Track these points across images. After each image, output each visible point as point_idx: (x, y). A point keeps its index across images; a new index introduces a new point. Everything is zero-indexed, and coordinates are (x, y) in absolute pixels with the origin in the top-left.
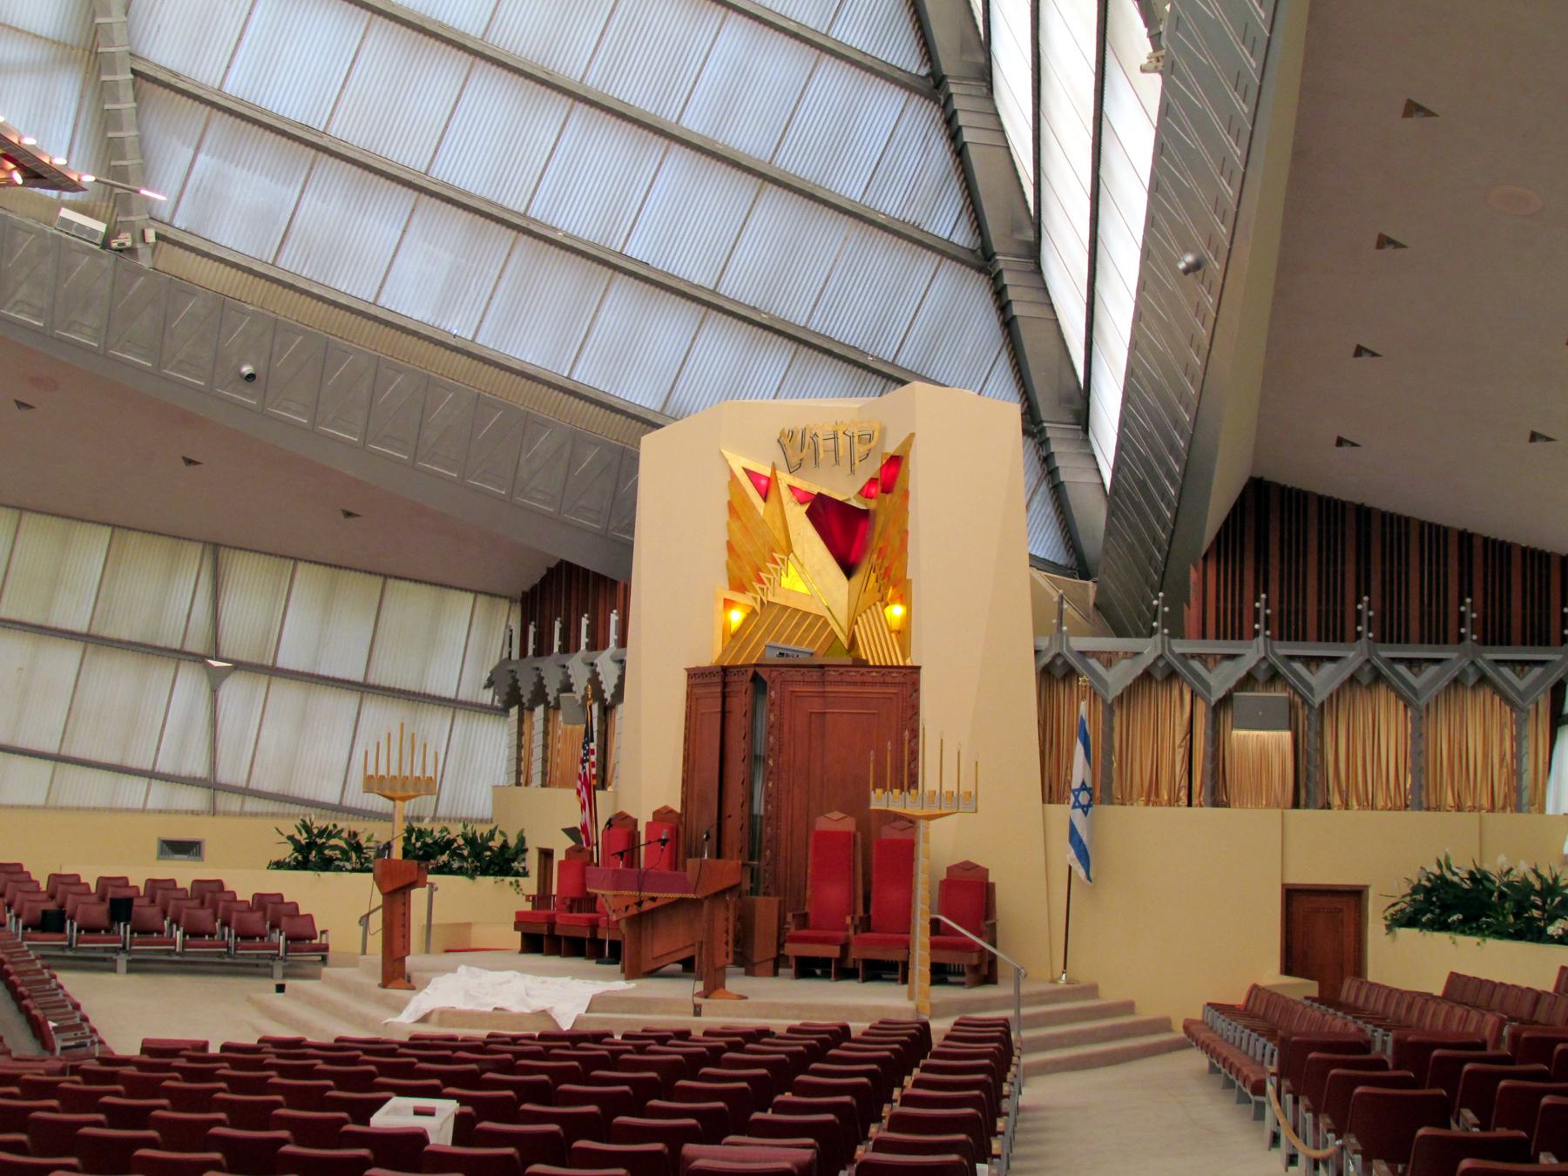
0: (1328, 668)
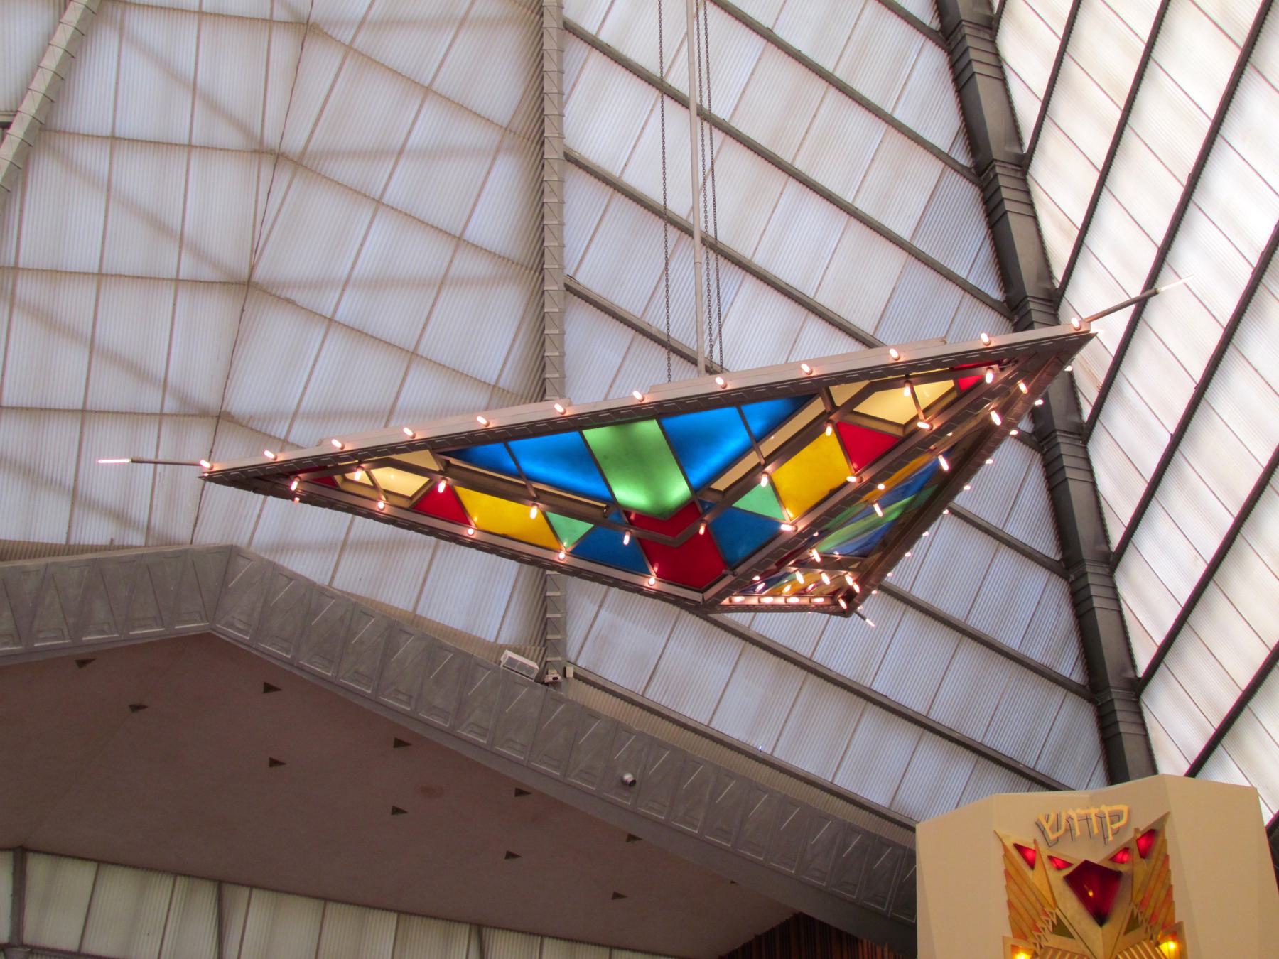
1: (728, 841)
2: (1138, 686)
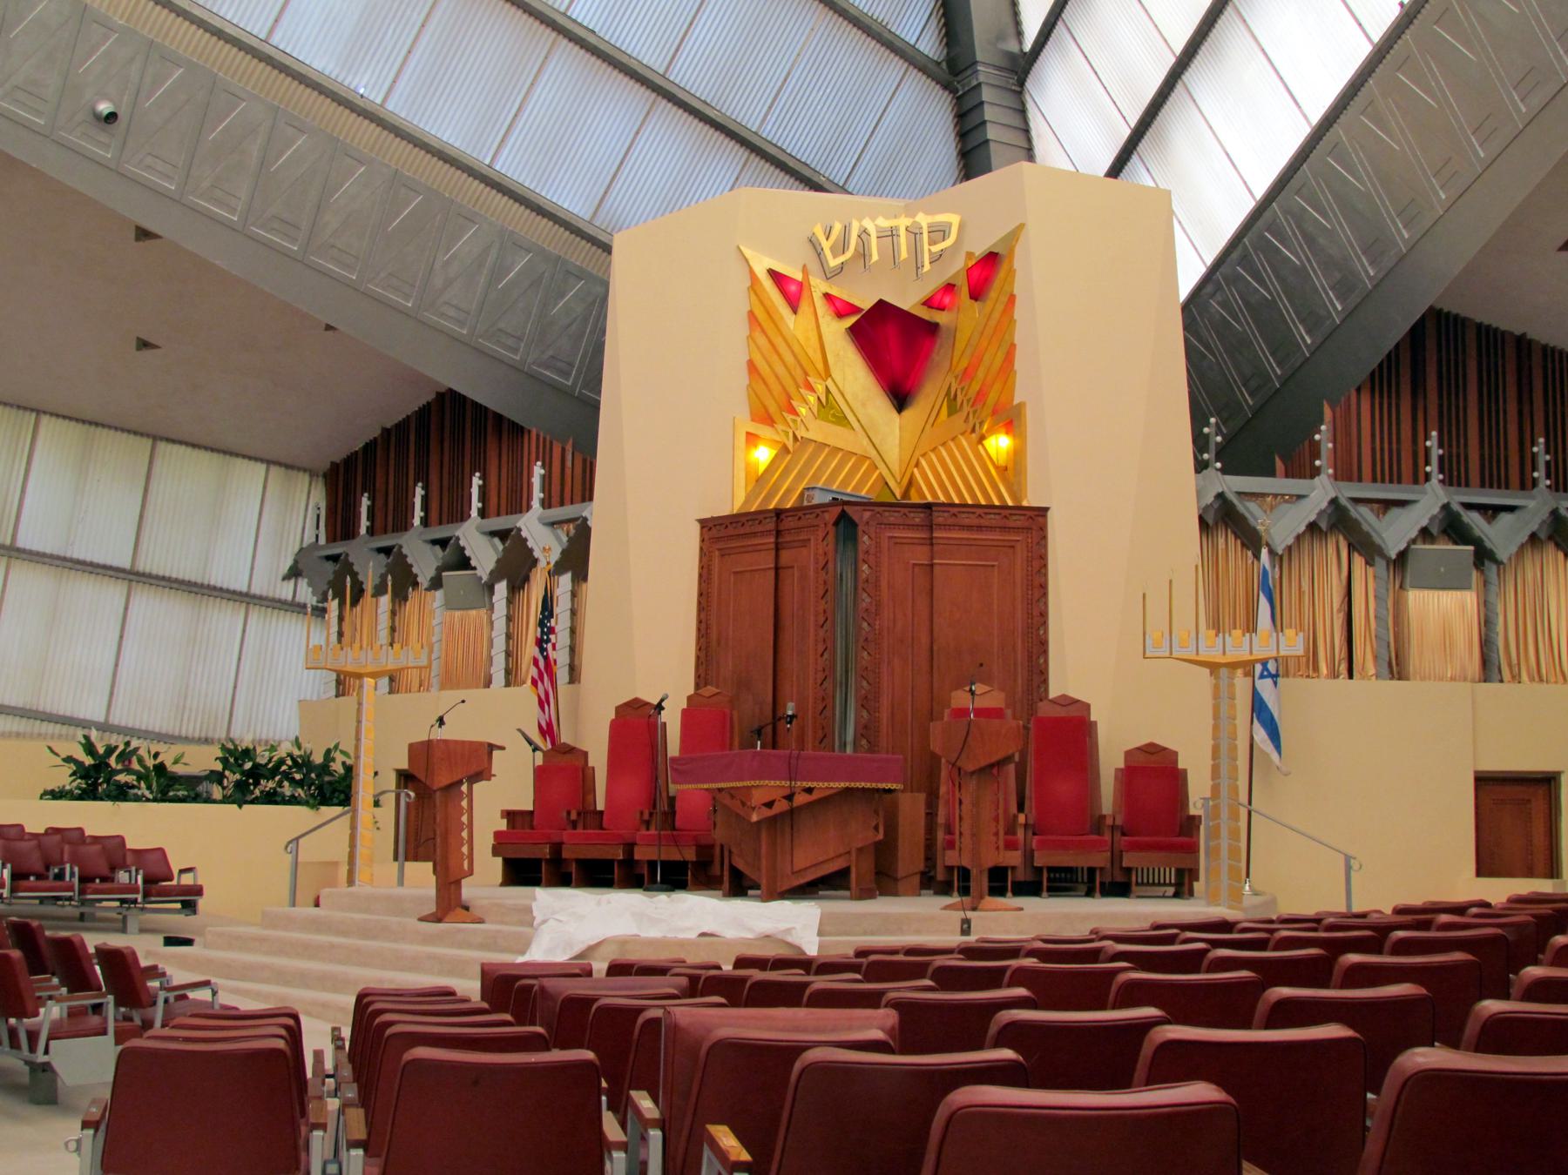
0: (1505, 518)
1: (294, 240)
2: (1021, 67)
